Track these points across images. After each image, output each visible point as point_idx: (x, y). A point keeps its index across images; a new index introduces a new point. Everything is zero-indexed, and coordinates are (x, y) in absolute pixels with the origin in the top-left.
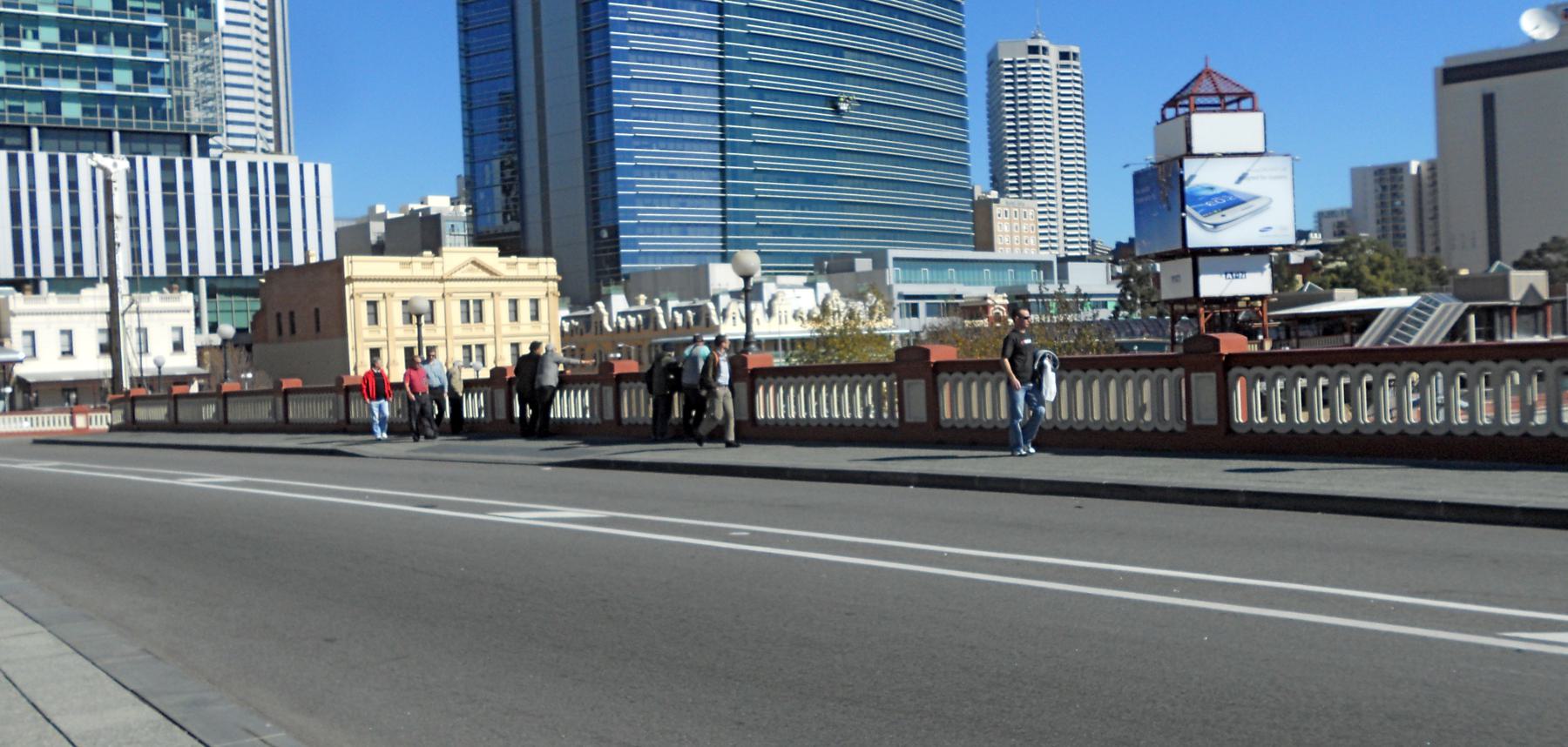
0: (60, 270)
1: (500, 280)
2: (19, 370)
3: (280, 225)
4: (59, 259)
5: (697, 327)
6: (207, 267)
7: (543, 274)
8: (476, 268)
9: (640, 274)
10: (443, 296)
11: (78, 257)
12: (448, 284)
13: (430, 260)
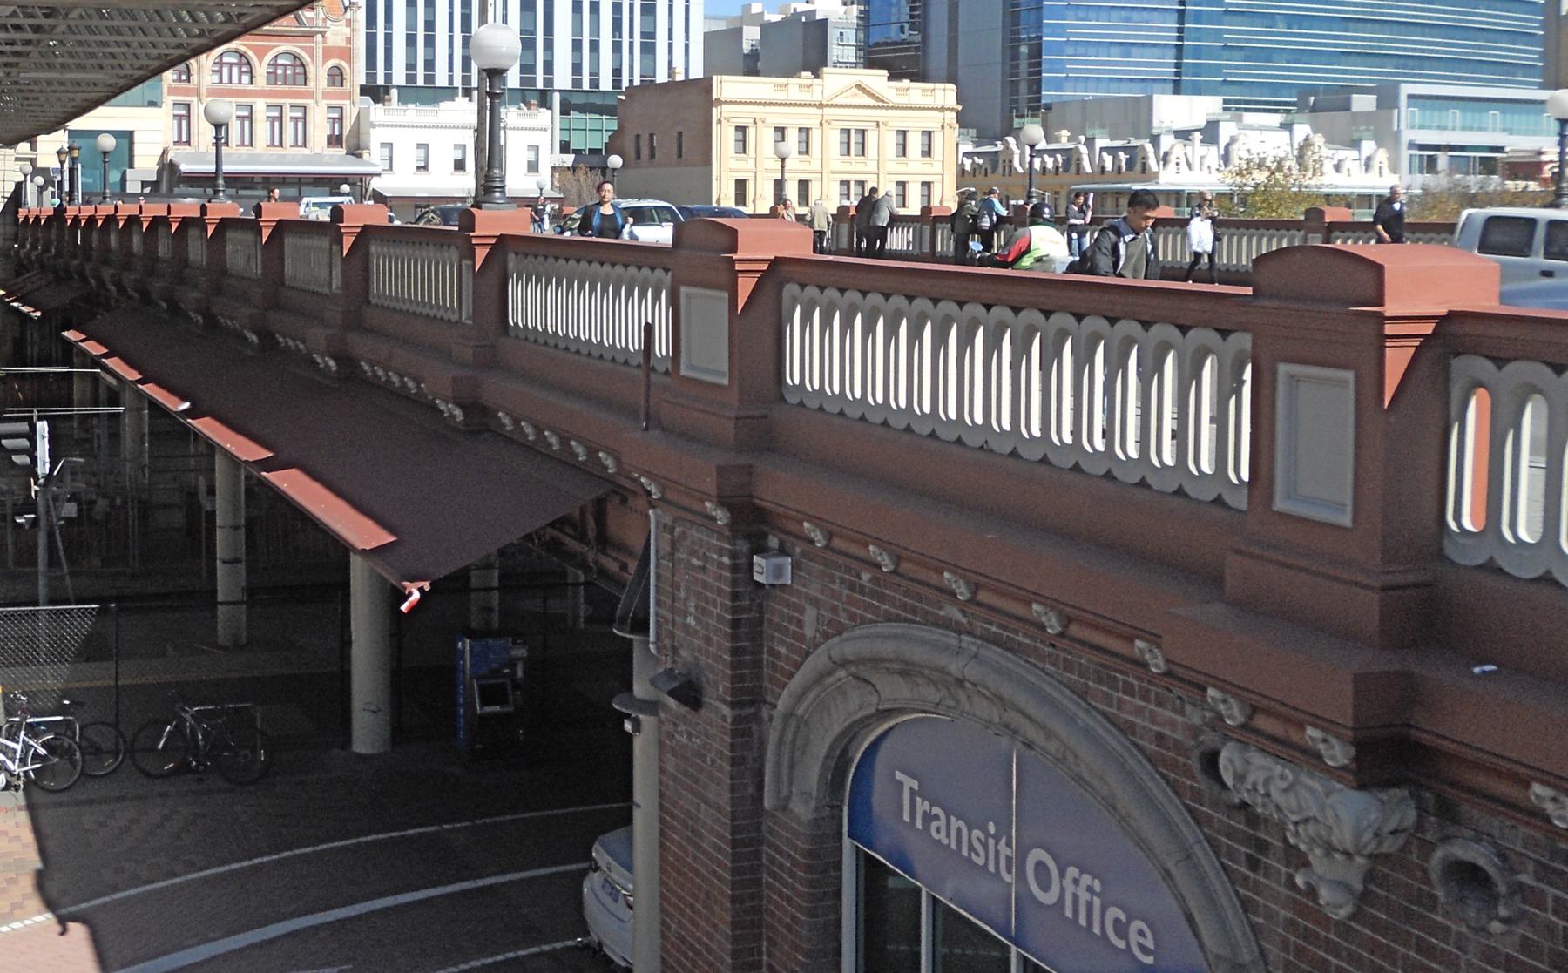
0: (411, 78)
1: (888, 108)
2: (375, 184)
3: (644, 35)
4: (411, 66)
5: (1132, 173)
6: (563, 79)
7: (939, 102)
8: (860, 93)
9: (1064, 104)
10: (821, 124)
11: (430, 65)
12: (827, 110)
13: (809, 82)
